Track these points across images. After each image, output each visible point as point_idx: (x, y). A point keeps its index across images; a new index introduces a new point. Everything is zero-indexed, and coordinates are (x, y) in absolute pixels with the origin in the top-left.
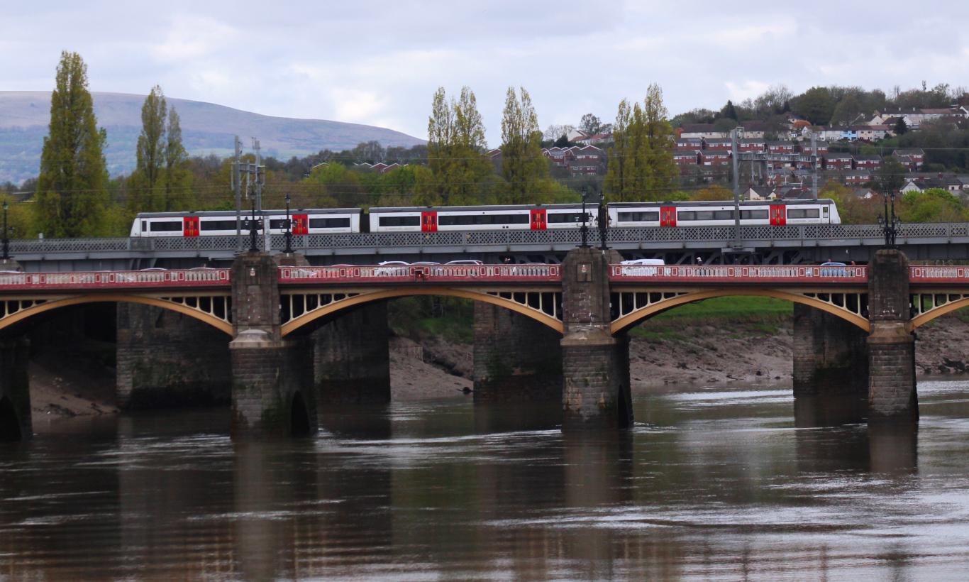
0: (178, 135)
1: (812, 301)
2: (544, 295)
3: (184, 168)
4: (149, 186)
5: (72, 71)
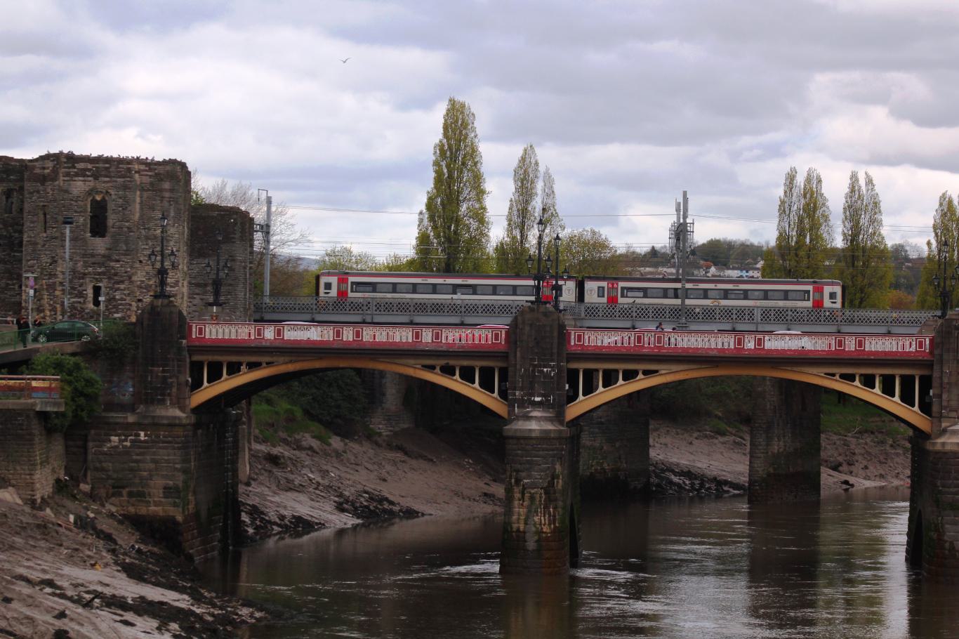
1: (452, 381)
2: (902, 377)
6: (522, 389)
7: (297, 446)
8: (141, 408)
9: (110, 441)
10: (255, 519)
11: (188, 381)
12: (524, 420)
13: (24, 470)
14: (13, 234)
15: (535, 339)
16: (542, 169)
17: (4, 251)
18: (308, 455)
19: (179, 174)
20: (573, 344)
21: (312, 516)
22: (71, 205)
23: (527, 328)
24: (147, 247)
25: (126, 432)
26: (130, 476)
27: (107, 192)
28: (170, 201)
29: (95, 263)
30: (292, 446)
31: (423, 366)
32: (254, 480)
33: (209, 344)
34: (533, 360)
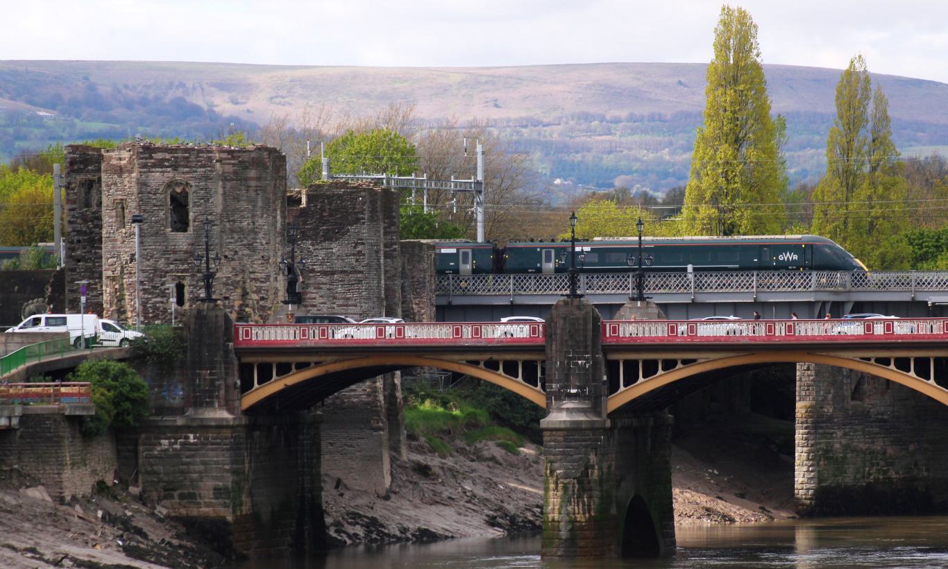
0: (887, 125)
3: (895, 174)
4: (844, 199)
5: (737, 34)
6: (557, 382)
7: (478, 457)
8: (190, 412)
9: (160, 444)
10: (371, 532)
11: (236, 383)
12: (558, 412)
13: (53, 470)
14: (93, 230)
15: (569, 332)
17: (85, 248)
18: (488, 466)
19: (266, 160)
20: (608, 336)
21: (447, 530)
22: (150, 199)
23: (562, 321)
24: (232, 241)
25: (175, 435)
26: (181, 478)
27: (187, 184)
28: (256, 191)
29: (176, 260)
30: (471, 456)
31: (861, 358)
32: (395, 493)
33: (255, 346)
34: (568, 352)
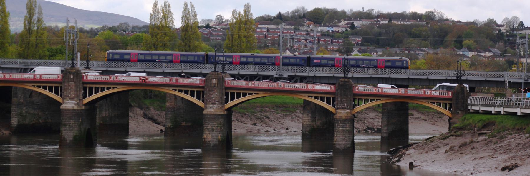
2: (197, 91)
16: (38, 4)
